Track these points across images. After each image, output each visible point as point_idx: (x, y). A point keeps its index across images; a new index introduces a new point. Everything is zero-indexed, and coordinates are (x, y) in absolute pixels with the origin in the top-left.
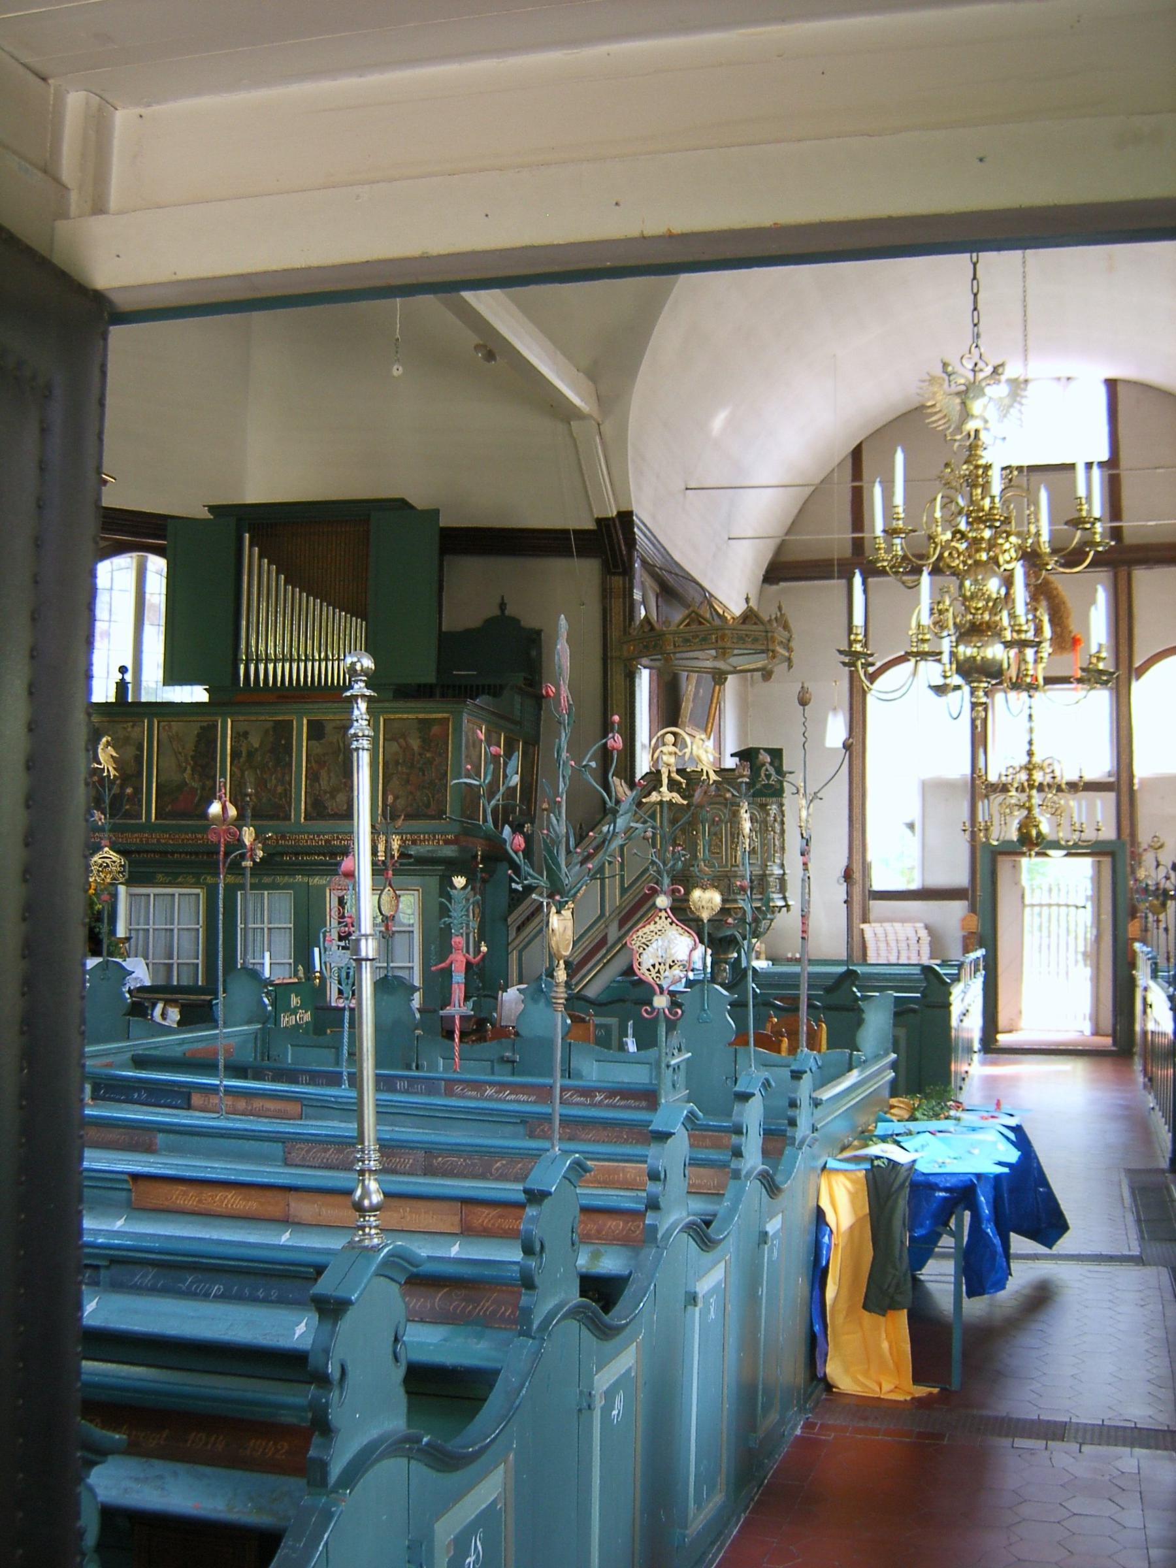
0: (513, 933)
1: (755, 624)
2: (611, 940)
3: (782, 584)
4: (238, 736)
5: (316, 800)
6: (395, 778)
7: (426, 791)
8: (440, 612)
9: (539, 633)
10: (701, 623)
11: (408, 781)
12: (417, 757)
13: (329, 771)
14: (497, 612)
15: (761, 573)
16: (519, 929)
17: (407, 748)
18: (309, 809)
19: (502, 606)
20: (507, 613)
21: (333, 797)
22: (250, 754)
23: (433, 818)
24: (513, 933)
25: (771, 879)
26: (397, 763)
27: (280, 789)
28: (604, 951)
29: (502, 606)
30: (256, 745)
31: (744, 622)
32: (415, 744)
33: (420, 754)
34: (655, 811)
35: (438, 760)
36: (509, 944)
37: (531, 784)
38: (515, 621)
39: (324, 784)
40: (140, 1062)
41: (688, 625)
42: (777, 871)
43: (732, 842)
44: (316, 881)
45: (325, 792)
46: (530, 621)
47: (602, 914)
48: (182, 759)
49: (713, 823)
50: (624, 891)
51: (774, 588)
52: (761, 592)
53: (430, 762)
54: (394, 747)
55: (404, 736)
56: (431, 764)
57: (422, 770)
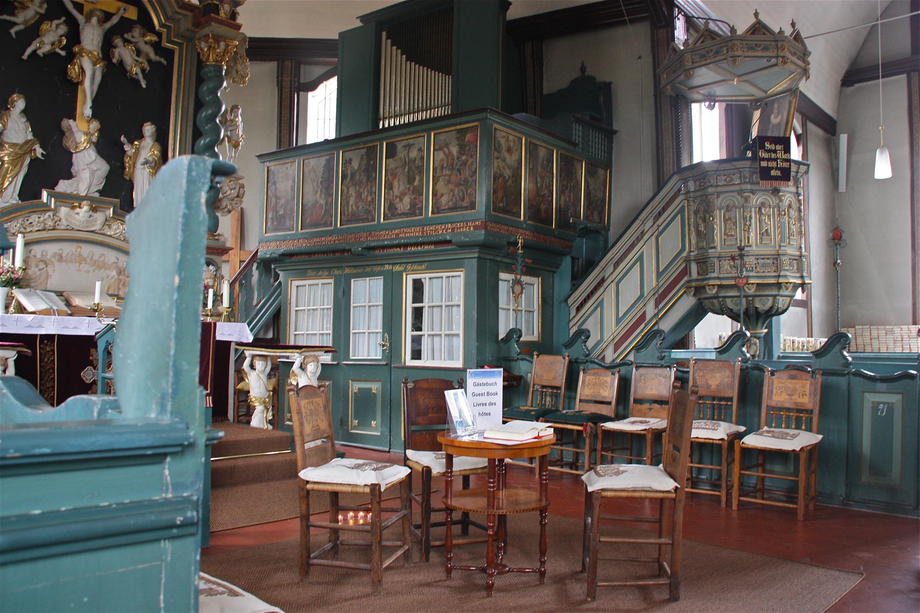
0: (573, 313)
1: (764, 34)
2: (648, 317)
3: (856, 85)
4: (347, 162)
5: (391, 204)
6: (441, 179)
7: (462, 187)
8: (914, 304)
9: (610, 83)
10: (713, 39)
11: (449, 182)
12: (456, 161)
13: (399, 181)
14: (580, 74)
15: (840, 83)
16: (578, 309)
17: (449, 155)
18: (387, 211)
19: (583, 69)
20: (586, 74)
21: (401, 200)
22: (353, 175)
23: (466, 208)
24: (573, 313)
25: (783, 258)
26: (442, 168)
27: (369, 199)
28: (643, 326)
29: (583, 69)
30: (356, 168)
31: (753, 33)
32: (455, 150)
33: (458, 158)
34: (683, 207)
35: (470, 161)
36: (570, 321)
37: (604, 200)
38: (592, 79)
39: (396, 191)
40: (646, 422)
41: (703, 42)
42: (792, 251)
43: (745, 225)
44: (397, 268)
45: (397, 197)
46: (602, 77)
47: (642, 295)
48: (315, 184)
49: (728, 209)
50: (659, 274)
51: (851, 89)
52: (841, 92)
53: (465, 163)
54: (441, 155)
55: (447, 145)
56: (465, 164)
57: (459, 170)
